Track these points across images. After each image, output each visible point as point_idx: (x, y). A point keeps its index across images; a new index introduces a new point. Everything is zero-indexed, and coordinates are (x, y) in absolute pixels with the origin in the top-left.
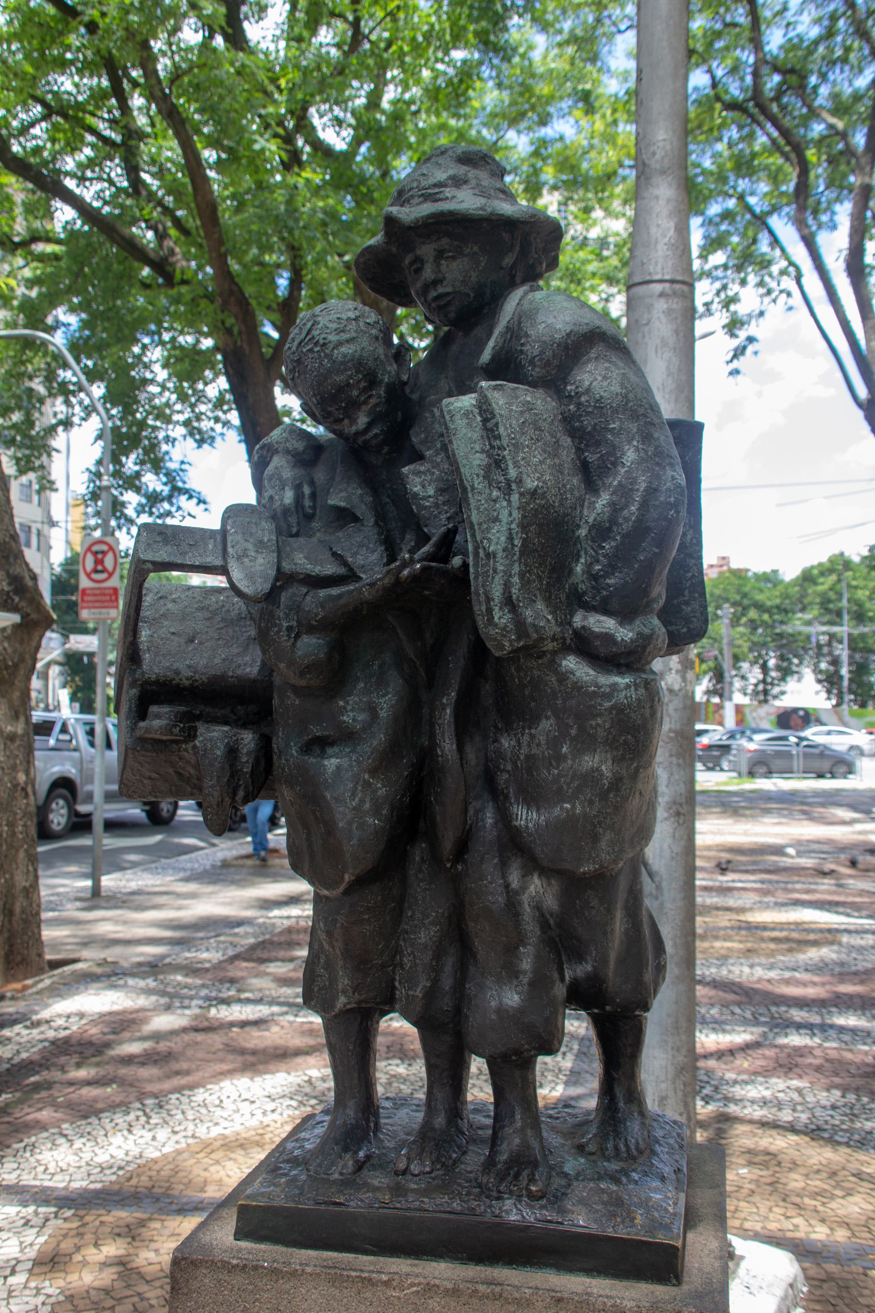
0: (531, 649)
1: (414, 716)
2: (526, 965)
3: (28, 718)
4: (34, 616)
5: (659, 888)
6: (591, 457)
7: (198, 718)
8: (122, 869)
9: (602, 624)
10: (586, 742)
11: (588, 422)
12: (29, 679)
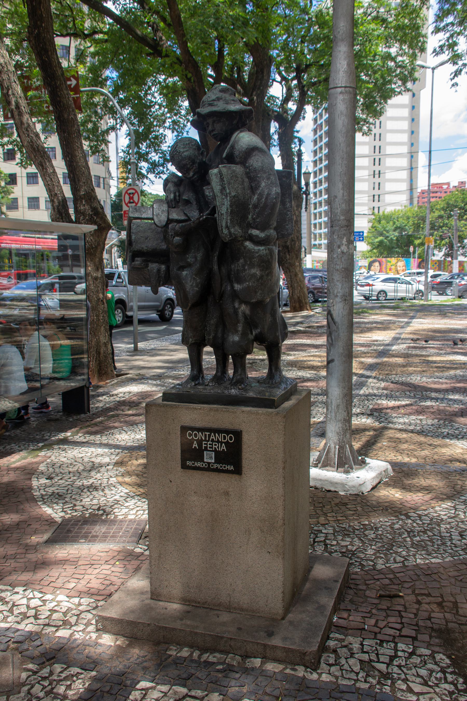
0: (234, 240)
1: (207, 259)
2: (240, 329)
3: (103, 272)
4: (103, 225)
5: (338, 328)
6: (253, 185)
7: (149, 261)
8: (147, 340)
9: (255, 232)
10: (252, 266)
11: (252, 175)
12: (102, 253)
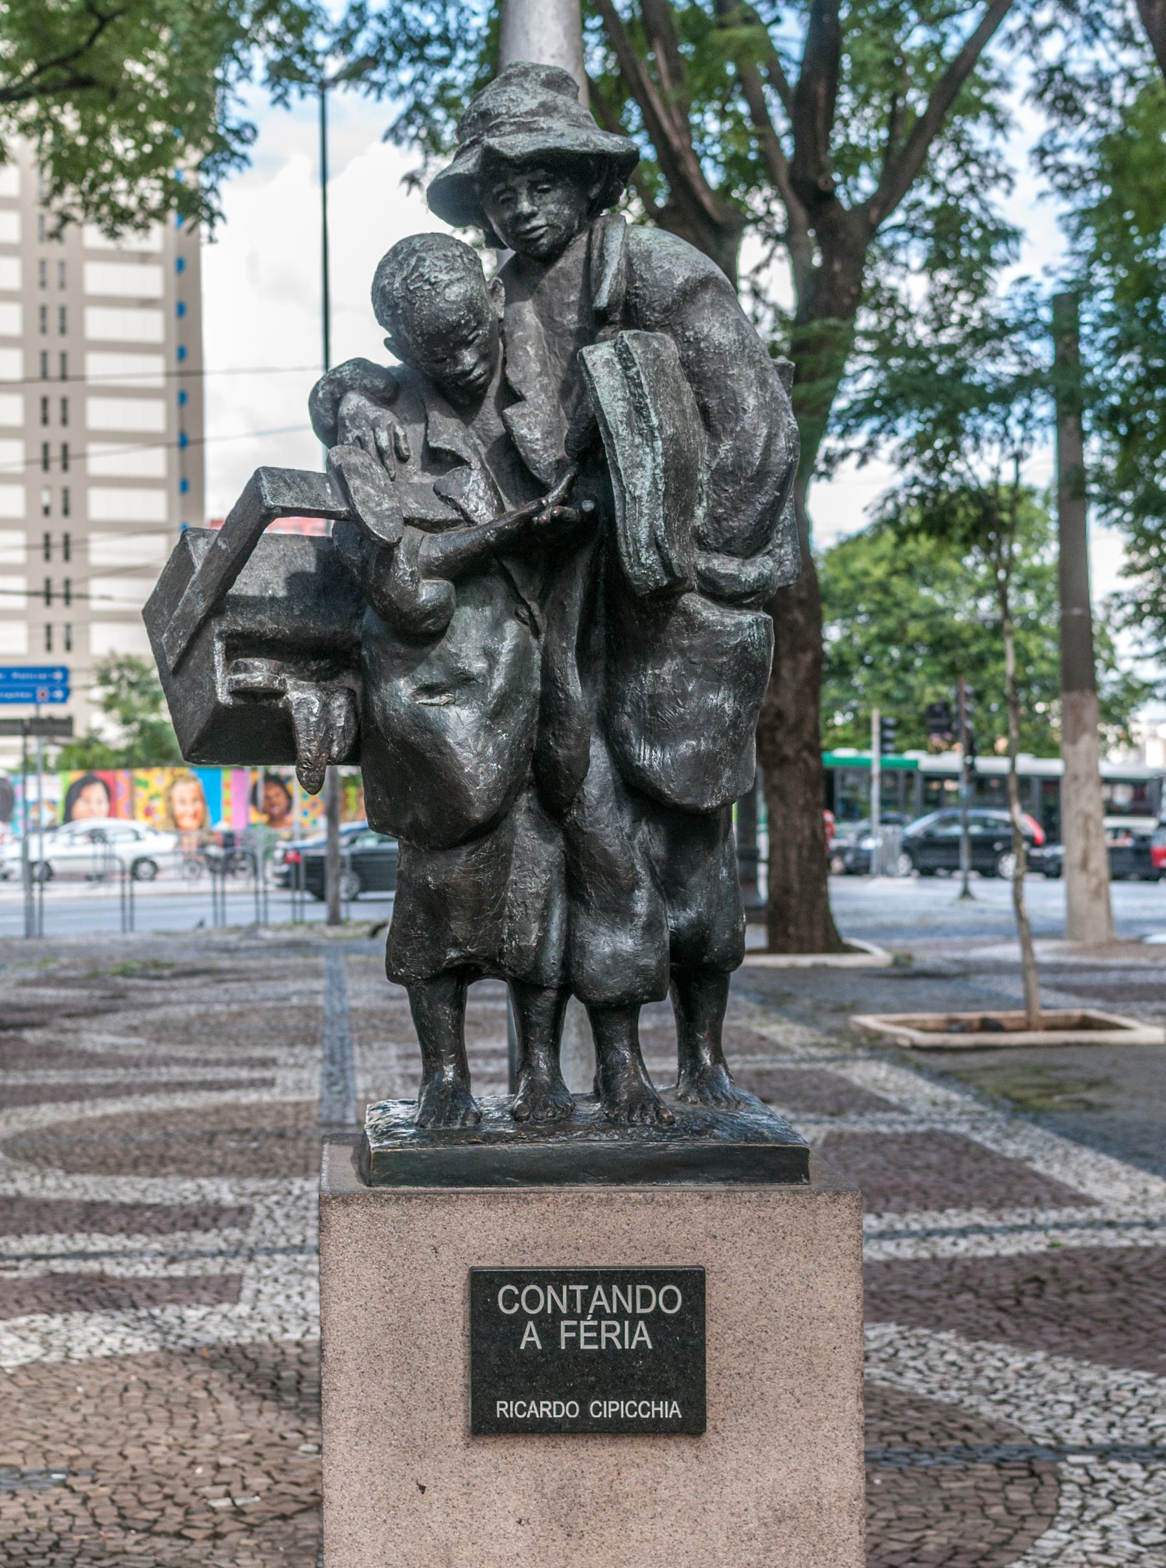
6: (713, 403)
9: (723, 565)
11: (709, 367)
